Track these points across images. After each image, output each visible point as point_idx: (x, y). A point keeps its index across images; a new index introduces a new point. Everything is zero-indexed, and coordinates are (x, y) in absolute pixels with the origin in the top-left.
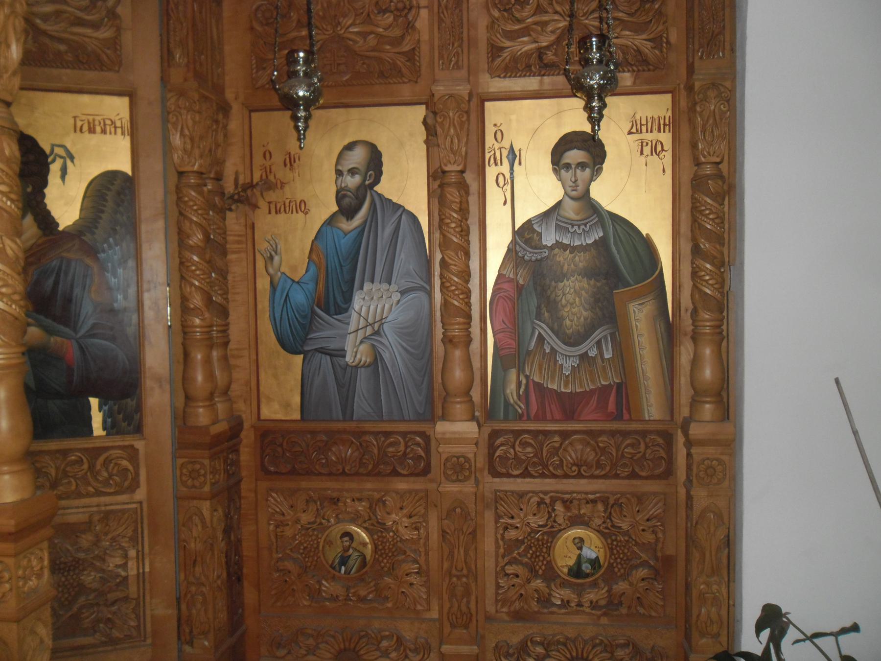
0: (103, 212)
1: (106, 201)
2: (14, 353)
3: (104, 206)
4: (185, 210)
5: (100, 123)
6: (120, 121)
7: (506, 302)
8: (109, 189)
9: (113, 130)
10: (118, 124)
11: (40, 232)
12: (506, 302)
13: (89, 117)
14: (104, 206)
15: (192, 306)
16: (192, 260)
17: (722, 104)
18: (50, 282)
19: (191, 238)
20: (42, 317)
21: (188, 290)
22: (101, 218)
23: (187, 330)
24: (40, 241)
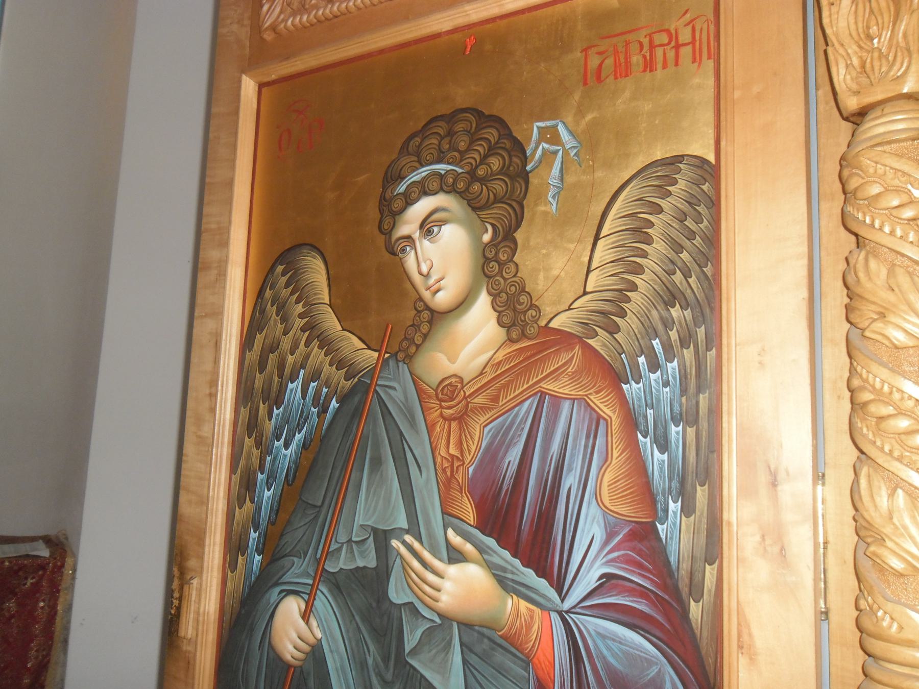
0: (638, 270)
1: (648, 241)
2: (905, 319)
3: (645, 255)
4: (872, 225)
5: (641, 45)
6: (689, 28)
7: (865, 10)
8: (659, 210)
9: (671, 54)
10: (685, 36)
11: (501, 333)
12: (865, 10)
13: (615, 40)
14: (645, 255)
15: (896, 564)
16: (896, 396)
17: (535, 316)
18: (514, 456)
19: (892, 318)
20: (491, 542)
21: (883, 501)
22: (634, 287)
23: (876, 646)
24: (500, 356)
